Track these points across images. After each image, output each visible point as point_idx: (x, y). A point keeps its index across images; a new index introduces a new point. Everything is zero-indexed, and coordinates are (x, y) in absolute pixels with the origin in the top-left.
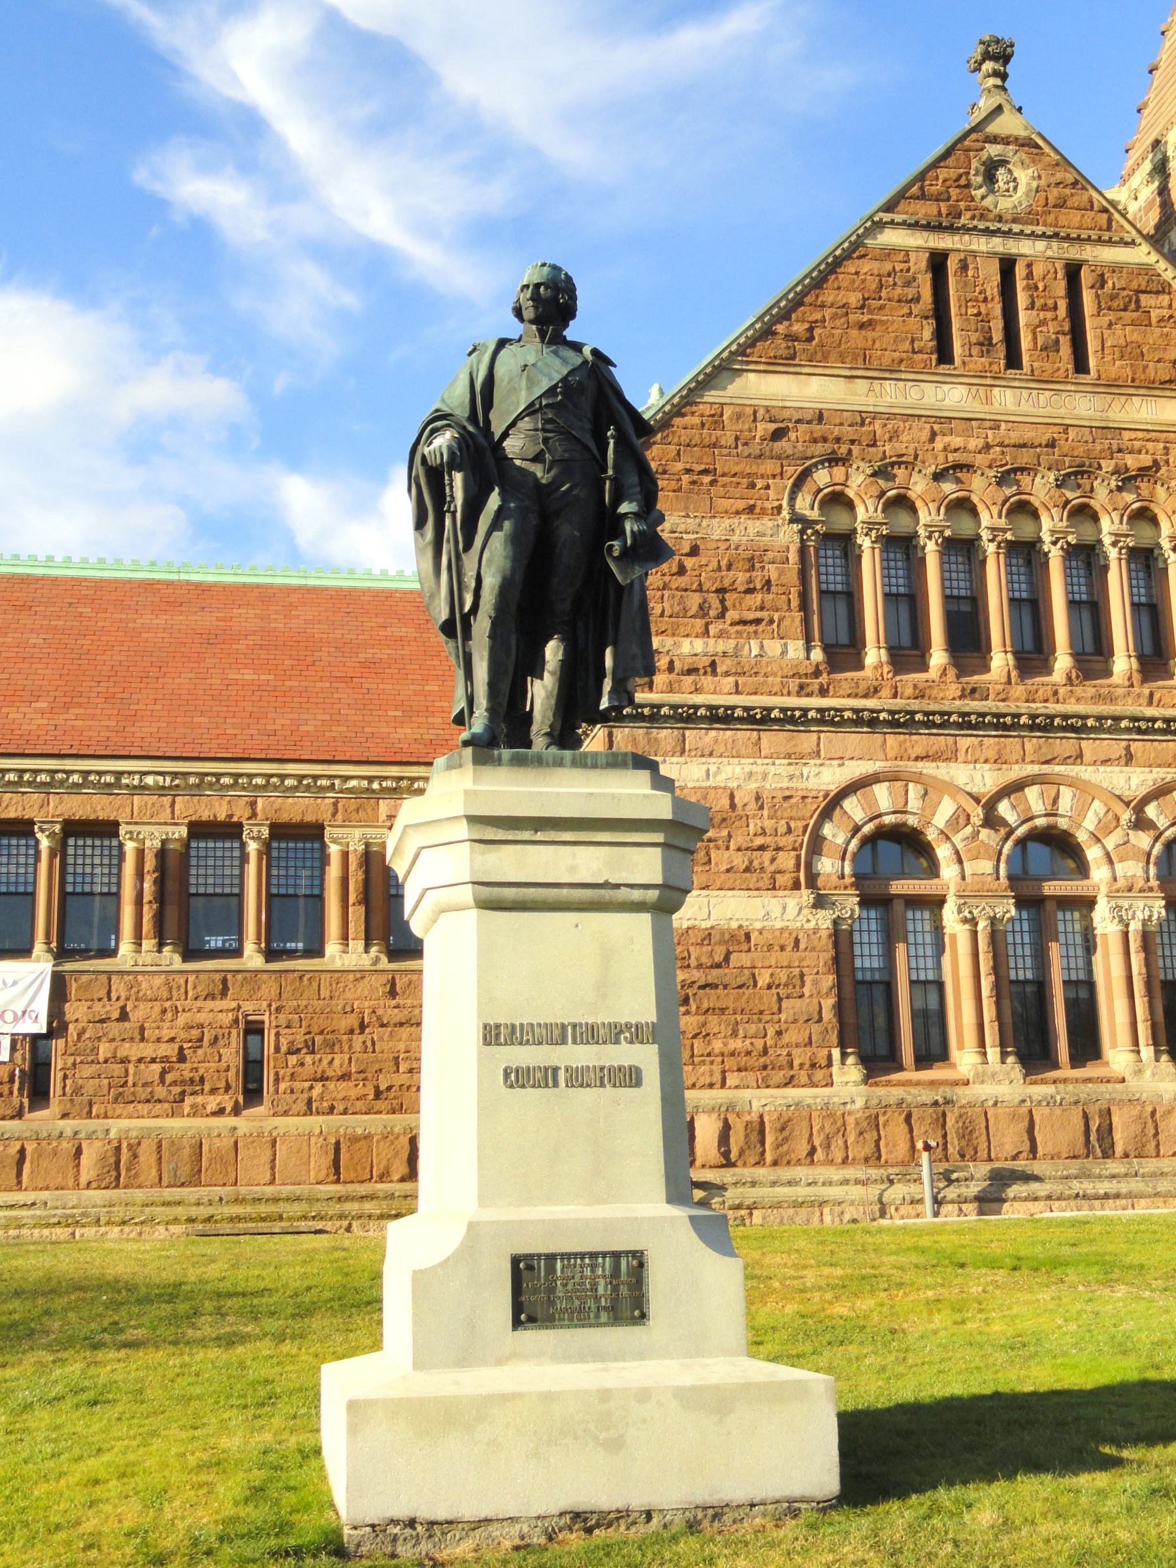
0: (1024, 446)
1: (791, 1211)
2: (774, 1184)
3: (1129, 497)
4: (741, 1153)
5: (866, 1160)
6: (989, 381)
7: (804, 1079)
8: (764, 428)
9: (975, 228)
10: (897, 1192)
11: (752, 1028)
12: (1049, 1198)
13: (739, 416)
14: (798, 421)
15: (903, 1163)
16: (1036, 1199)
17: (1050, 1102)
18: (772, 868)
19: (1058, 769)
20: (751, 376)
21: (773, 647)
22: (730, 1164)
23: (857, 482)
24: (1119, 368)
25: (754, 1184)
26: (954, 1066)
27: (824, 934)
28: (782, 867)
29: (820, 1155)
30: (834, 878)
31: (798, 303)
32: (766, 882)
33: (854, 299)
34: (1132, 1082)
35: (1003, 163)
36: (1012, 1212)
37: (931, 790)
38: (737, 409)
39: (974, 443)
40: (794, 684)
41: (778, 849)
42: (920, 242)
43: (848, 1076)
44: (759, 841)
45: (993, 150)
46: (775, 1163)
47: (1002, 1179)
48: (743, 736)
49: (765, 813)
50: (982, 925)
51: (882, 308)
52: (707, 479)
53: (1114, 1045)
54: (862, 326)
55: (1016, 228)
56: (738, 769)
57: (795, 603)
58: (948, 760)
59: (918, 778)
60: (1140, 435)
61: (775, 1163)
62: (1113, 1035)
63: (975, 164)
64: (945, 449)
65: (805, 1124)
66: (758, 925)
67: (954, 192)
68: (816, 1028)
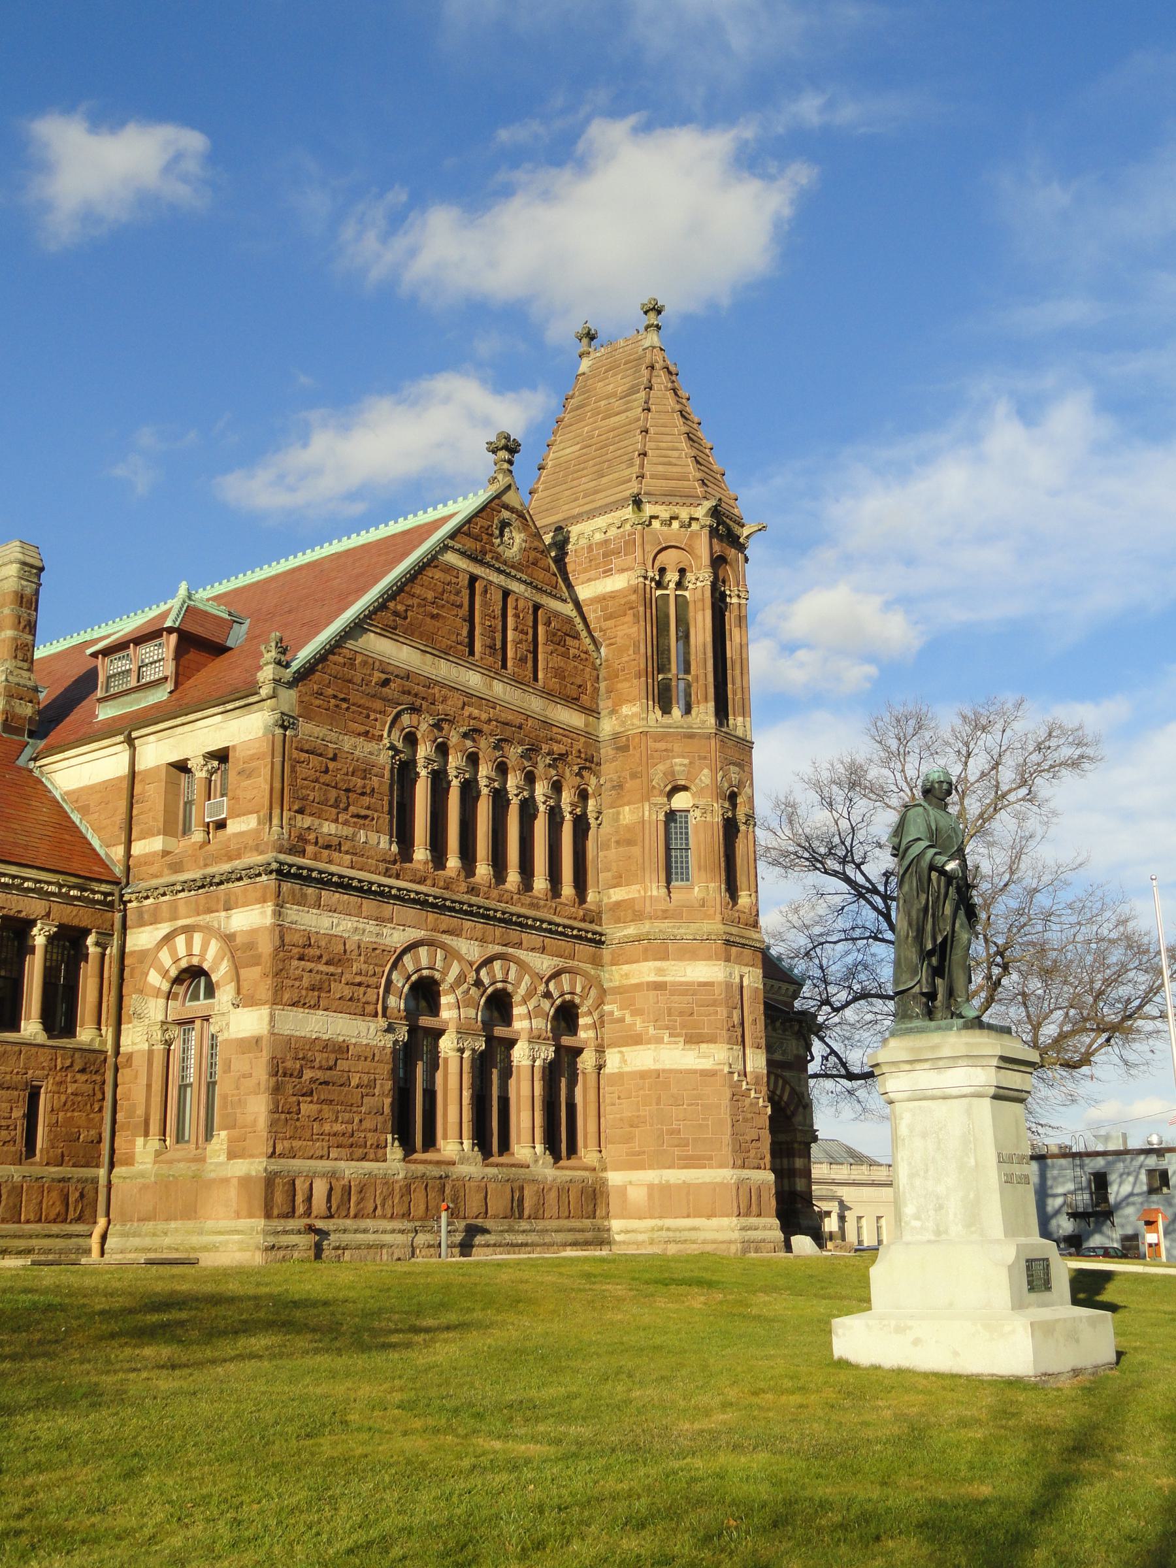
0: (507, 724)
1: (365, 1251)
2: (356, 1231)
3: (469, 743)
4: (338, 1208)
5: (403, 1215)
6: (492, 675)
7: (372, 1156)
8: (378, 676)
9: (493, 566)
10: (421, 1239)
11: (347, 1116)
12: (495, 1245)
13: (364, 663)
14: (397, 676)
15: (420, 1219)
16: (488, 1246)
17: (495, 1179)
18: (364, 1000)
19: (511, 950)
20: (372, 635)
21: (373, 837)
22: (331, 1217)
23: (424, 727)
24: (554, 683)
25: (345, 1231)
26: (439, 1150)
27: (388, 1051)
28: (369, 1000)
29: (379, 1212)
30: (396, 1011)
31: (401, 590)
32: (359, 1011)
33: (430, 595)
34: (533, 1168)
35: (509, 525)
36: (479, 1255)
37: (451, 954)
38: (365, 658)
39: (484, 716)
40: (382, 866)
41: (368, 986)
42: (464, 566)
43: (395, 1152)
44: (358, 979)
45: (506, 514)
46: (355, 1217)
47: (473, 1231)
48: (353, 900)
49: (362, 958)
50: (466, 1054)
51: (443, 606)
52: (345, 705)
53: (518, 1143)
54: (433, 617)
55: (513, 572)
56: (350, 924)
57: (386, 808)
58: (457, 935)
59: (443, 946)
60: (561, 731)
61: (355, 1217)
62: (519, 1136)
63: (496, 521)
64: (469, 716)
65: (373, 1189)
66: (353, 1041)
67: (485, 537)
68: (380, 1119)
